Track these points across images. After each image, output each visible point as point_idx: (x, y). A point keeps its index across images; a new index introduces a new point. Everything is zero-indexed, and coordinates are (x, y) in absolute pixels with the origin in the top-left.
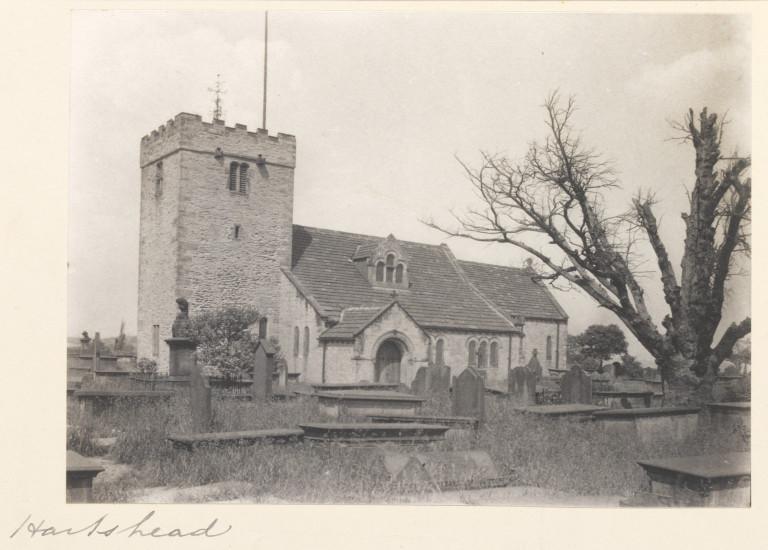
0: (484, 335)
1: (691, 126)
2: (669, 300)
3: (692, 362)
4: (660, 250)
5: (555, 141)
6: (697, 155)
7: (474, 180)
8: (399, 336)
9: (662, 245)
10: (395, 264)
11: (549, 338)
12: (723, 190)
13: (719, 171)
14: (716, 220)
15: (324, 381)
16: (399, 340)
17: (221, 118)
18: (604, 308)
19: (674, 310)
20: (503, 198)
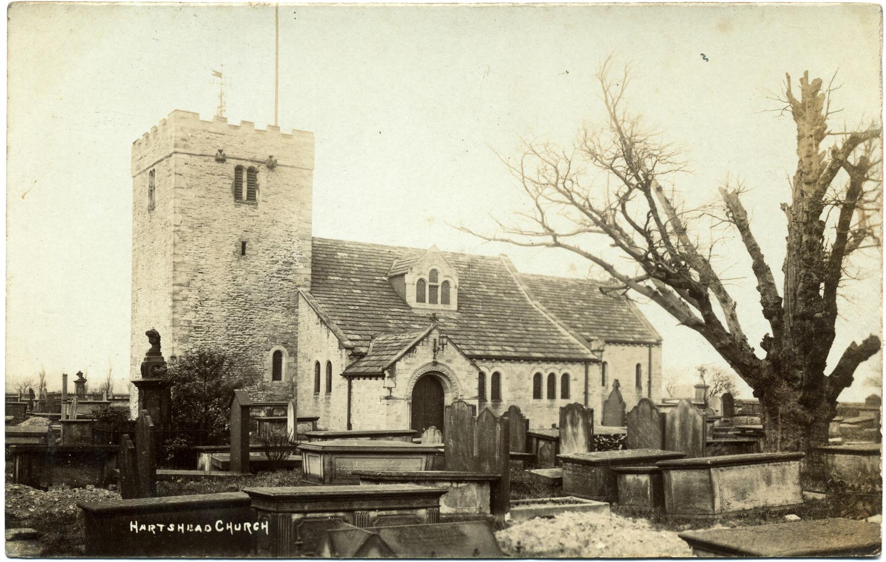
0: (552, 365)
1: (789, 94)
2: (768, 314)
3: (800, 395)
4: (753, 249)
5: (609, 119)
6: (799, 130)
7: (514, 172)
8: (439, 368)
9: (755, 245)
10: (440, 283)
11: (638, 366)
12: (833, 172)
13: (827, 150)
14: (826, 210)
15: (349, 426)
16: (441, 373)
17: (224, 115)
18: (685, 327)
19: (776, 327)
20: (549, 191)
